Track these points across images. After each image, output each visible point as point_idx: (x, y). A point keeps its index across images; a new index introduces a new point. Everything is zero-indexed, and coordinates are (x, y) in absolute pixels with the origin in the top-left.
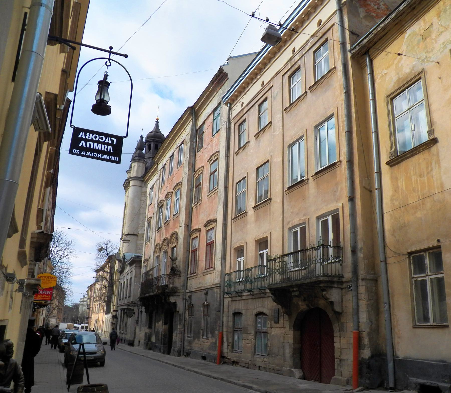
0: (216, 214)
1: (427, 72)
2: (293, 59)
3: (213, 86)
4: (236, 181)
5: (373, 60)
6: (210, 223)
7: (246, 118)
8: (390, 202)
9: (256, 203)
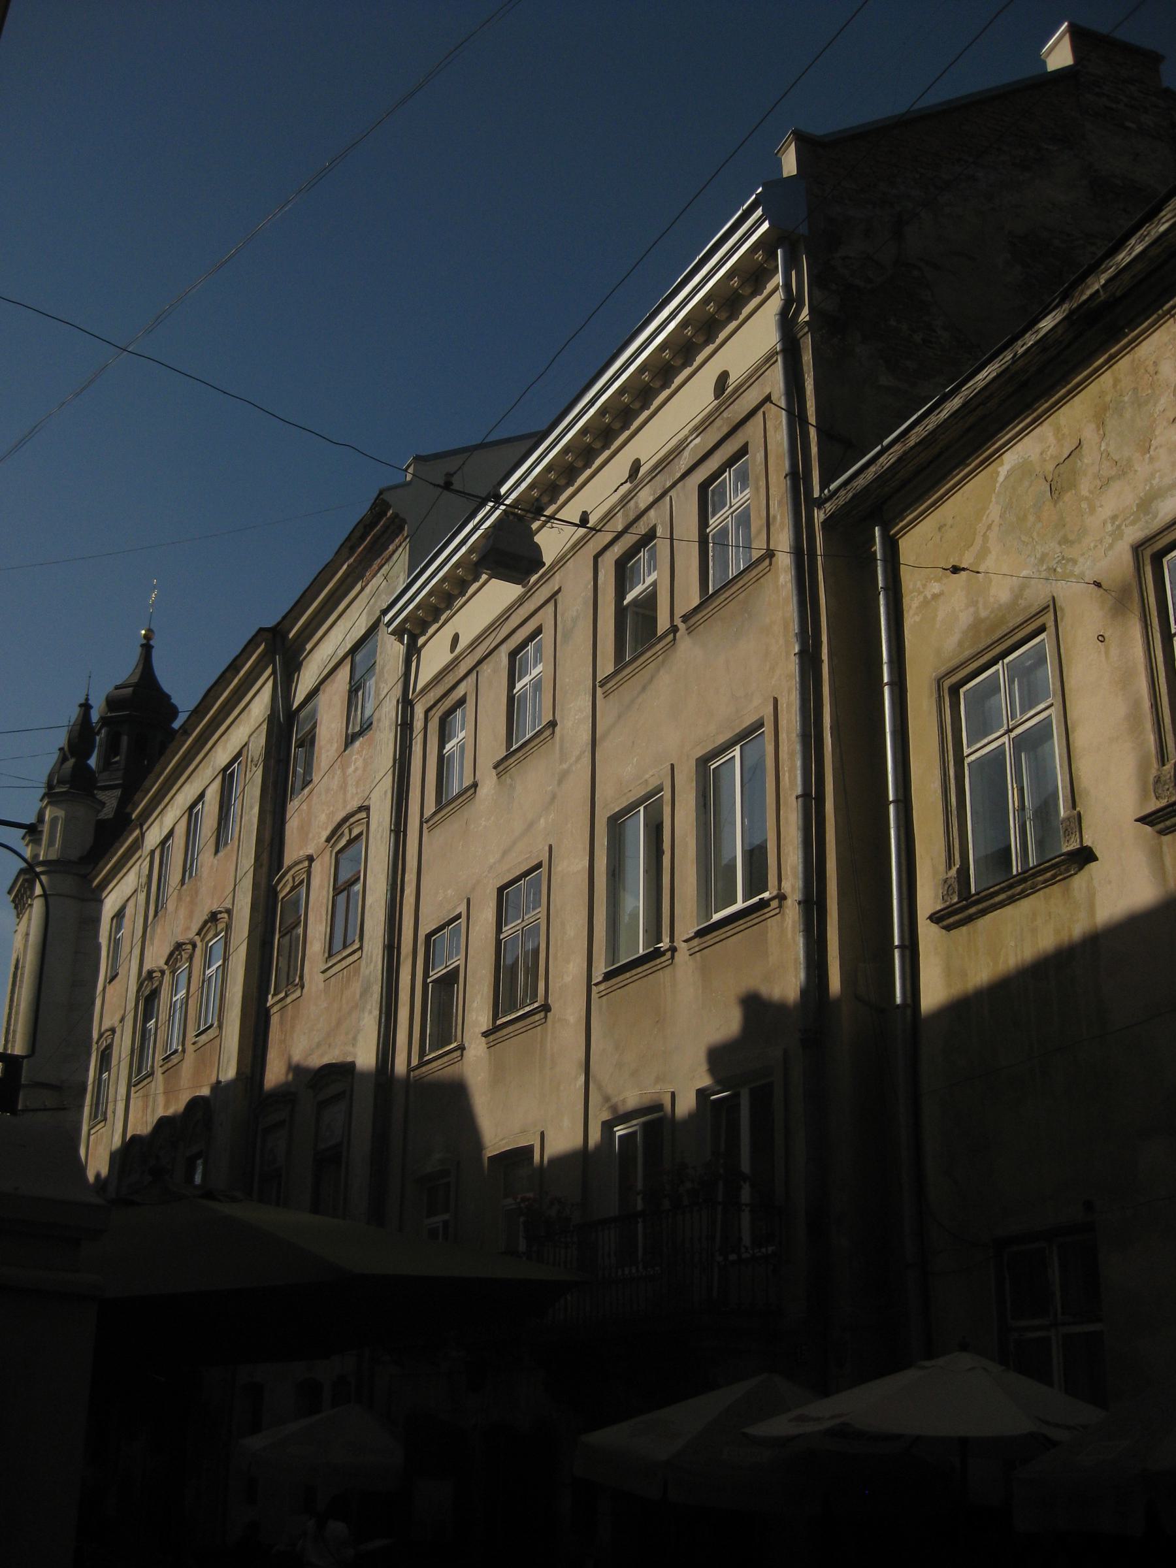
0: (354, 1045)
1: (1062, 610)
2: (632, 502)
3: (352, 560)
4: (423, 931)
9: (495, 1017)
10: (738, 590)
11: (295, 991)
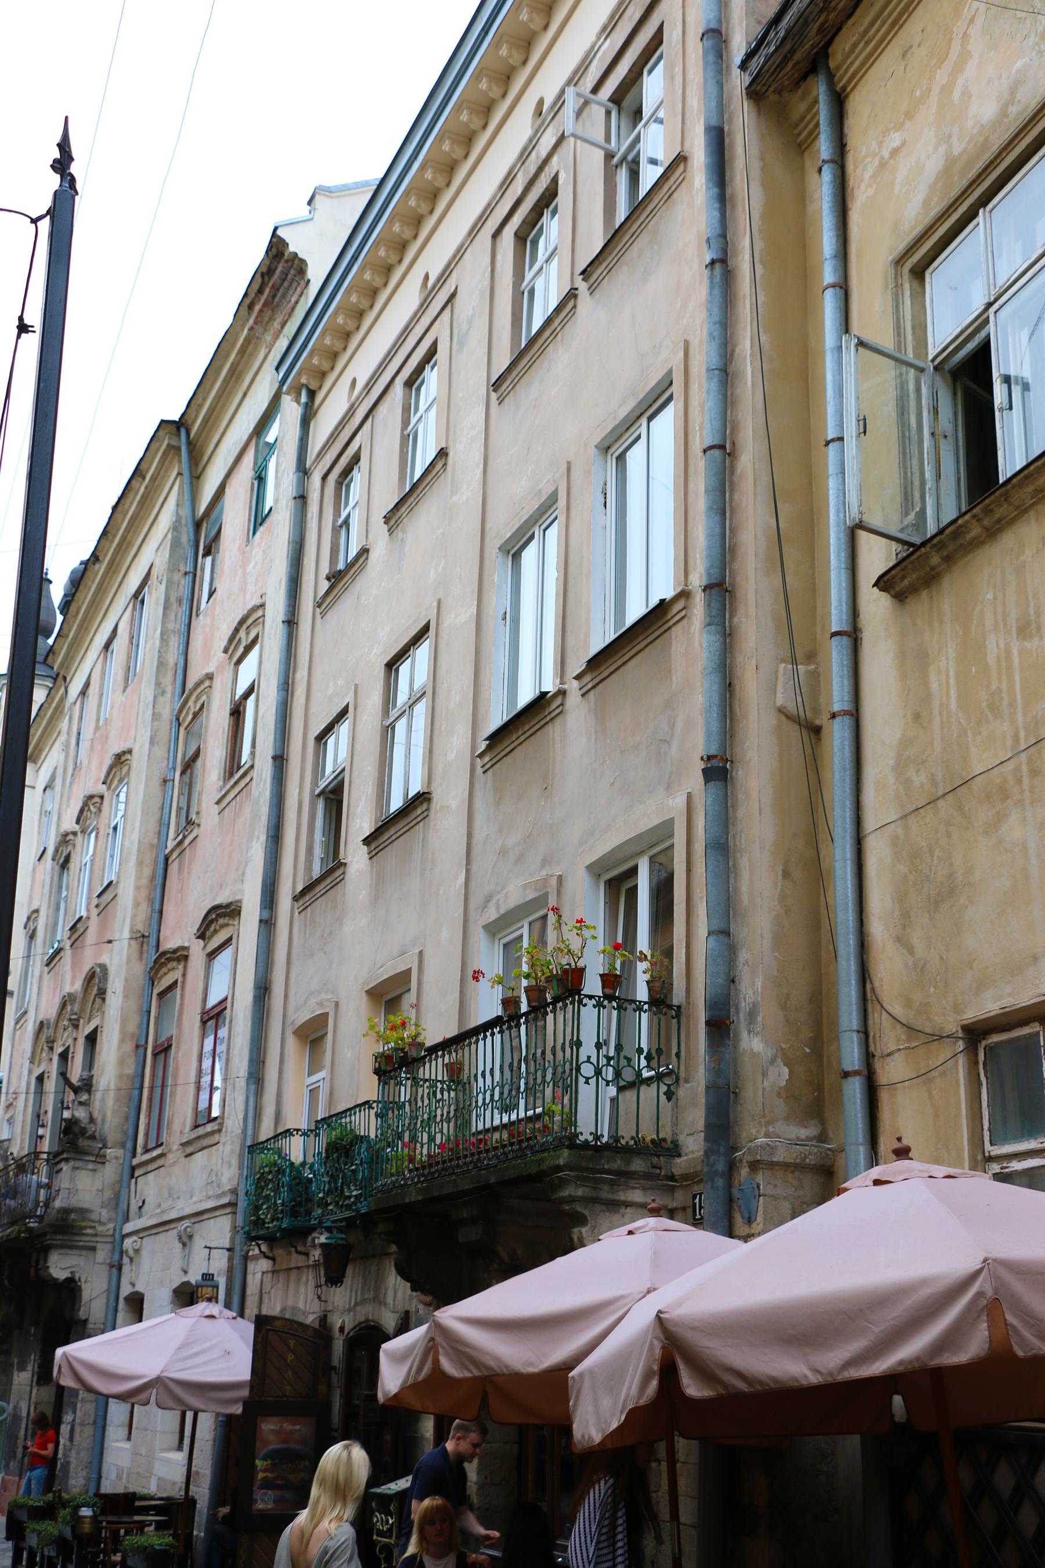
5: (847, 96)
6: (216, 920)
7: (436, 339)
8: (891, 780)
10: (648, 217)
11: (192, 831)
